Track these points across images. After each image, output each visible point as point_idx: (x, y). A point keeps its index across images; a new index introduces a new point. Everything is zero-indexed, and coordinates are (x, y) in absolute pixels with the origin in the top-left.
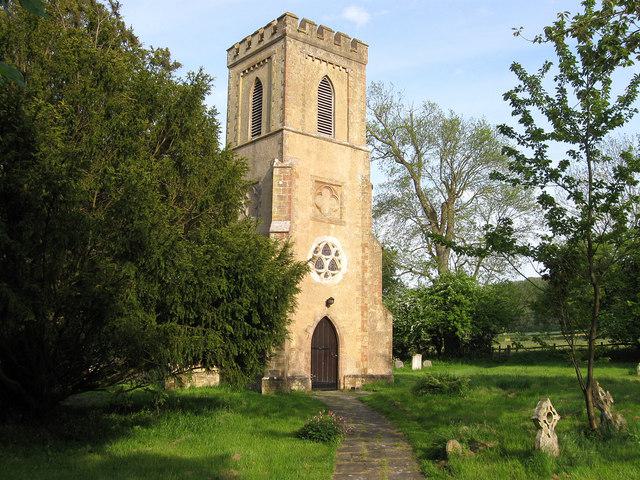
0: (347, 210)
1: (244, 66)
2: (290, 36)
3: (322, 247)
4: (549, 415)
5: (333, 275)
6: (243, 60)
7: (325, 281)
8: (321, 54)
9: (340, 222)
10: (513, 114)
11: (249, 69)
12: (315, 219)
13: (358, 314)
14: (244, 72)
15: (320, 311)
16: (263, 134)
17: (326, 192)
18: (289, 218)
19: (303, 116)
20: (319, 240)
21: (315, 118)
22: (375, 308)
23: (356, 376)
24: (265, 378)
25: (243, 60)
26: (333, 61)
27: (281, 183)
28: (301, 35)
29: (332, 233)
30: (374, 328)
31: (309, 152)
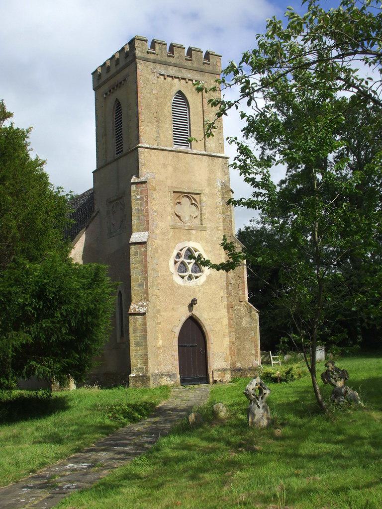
0: (207, 216)
1: (106, 88)
2: (141, 59)
3: (183, 252)
4: (133, 493)
5: (197, 277)
6: (105, 82)
7: (193, 282)
8: (172, 71)
9: (201, 228)
10: (242, 118)
11: (110, 91)
12: (174, 227)
13: (224, 312)
14: (106, 94)
15: (183, 314)
16: (124, 152)
17: (185, 201)
18: (147, 229)
19: (158, 133)
20: (180, 246)
21: (171, 132)
22: (240, 306)
23: (225, 370)
24: (131, 375)
25: (105, 82)
26: (185, 76)
27: (138, 197)
28: (152, 56)
29: (193, 238)
30: (240, 324)
31: (165, 165)
